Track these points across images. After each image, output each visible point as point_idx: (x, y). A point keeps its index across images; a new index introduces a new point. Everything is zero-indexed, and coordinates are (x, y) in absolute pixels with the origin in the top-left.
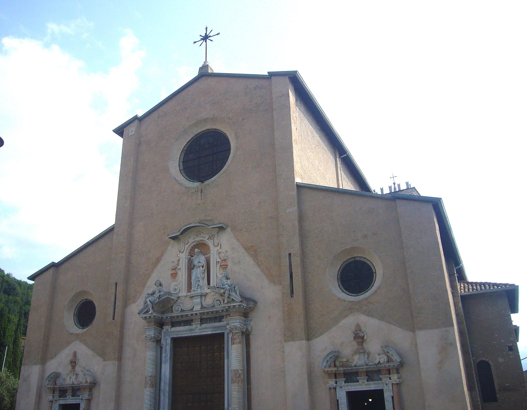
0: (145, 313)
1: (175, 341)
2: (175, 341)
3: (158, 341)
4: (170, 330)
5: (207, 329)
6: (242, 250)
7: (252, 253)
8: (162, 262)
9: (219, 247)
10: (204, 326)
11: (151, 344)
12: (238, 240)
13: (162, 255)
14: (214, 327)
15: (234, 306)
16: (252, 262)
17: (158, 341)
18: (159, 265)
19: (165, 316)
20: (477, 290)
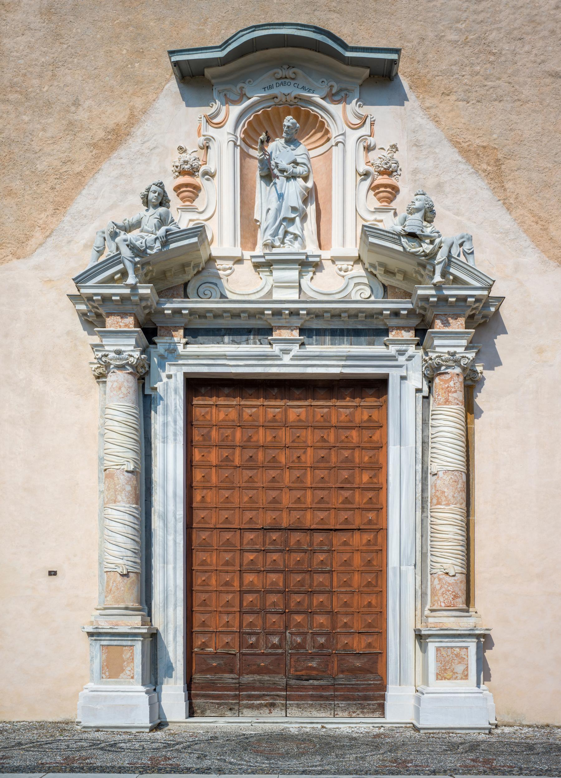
0: (111, 279)
1: (195, 385)
2: (195, 385)
3: (142, 377)
4: (180, 348)
5: (329, 358)
6: (449, 154)
7: (484, 166)
8: (134, 145)
9: (365, 131)
10: (313, 349)
11: (121, 382)
12: (436, 120)
13: (133, 120)
14: (349, 358)
15: (464, 299)
16: (486, 194)
17: (142, 377)
18: (122, 152)
19: (169, 306)
20: (432, 415)
